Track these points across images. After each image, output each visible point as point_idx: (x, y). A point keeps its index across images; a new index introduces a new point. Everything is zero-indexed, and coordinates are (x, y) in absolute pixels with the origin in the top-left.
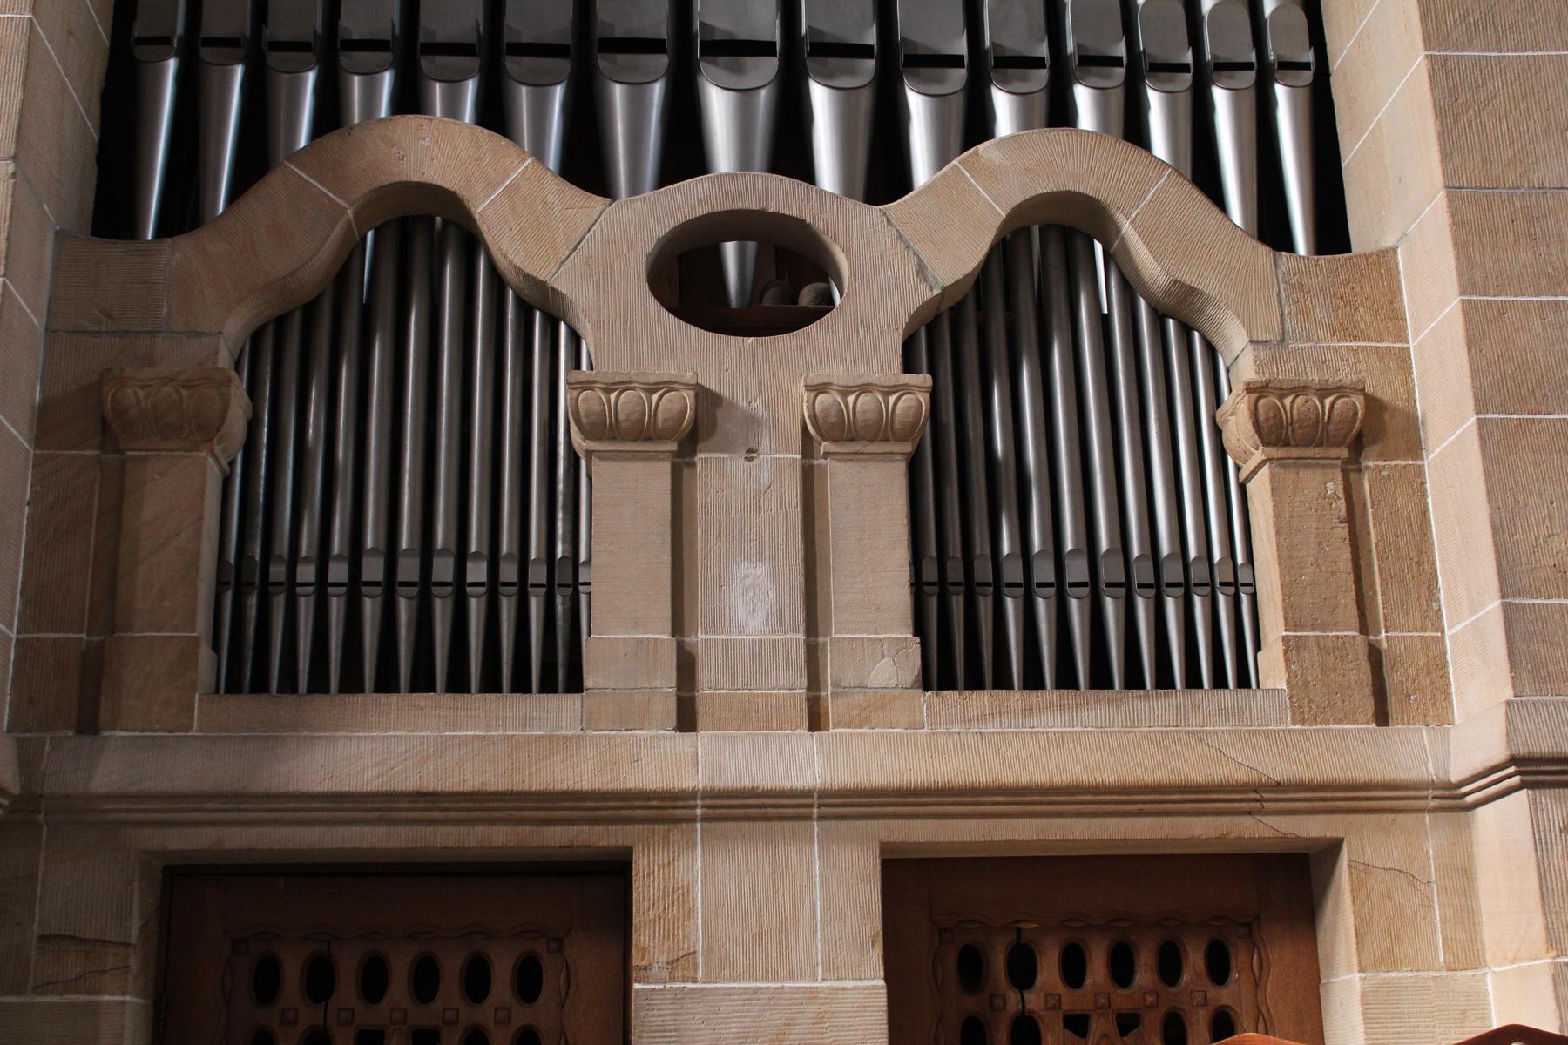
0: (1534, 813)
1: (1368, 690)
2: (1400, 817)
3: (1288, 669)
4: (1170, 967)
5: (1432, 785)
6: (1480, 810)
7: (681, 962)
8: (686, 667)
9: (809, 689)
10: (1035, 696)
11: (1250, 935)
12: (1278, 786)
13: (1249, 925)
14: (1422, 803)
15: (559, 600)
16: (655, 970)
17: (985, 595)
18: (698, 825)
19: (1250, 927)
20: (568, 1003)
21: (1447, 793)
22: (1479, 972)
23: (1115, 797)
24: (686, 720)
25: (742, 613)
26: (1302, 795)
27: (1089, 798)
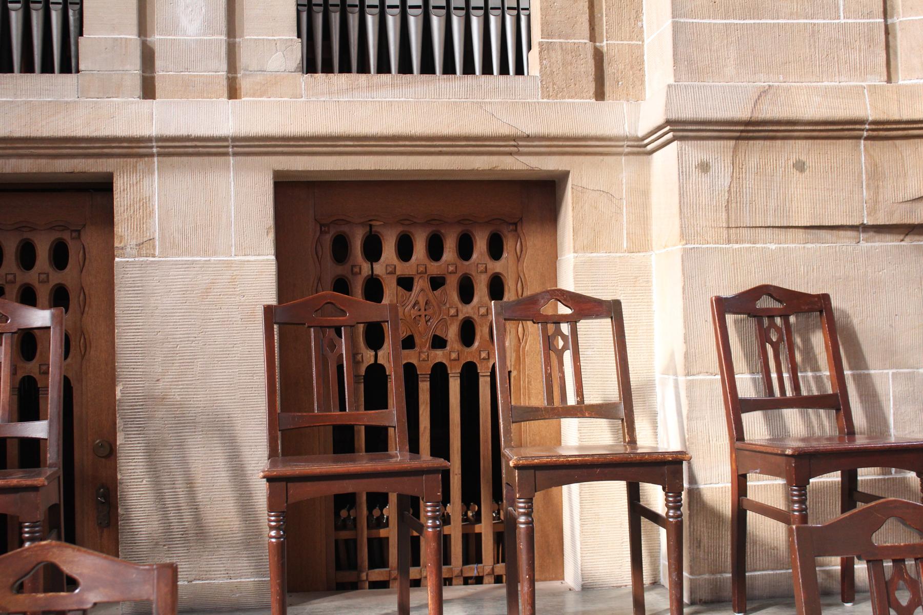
0: (680, 156)
1: (591, 78)
2: (606, 158)
3: (541, 63)
4: (465, 249)
5: (626, 138)
6: (655, 154)
7: (145, 245)
8: (148, 57)
10: (384, 77)
11: (516, 230)
12: (528, 138)
13: (516, 224)
14: (620, 150)
15: (71, 13)
16: (128, 250)
17: (353, 13)
19: (515, 224)
20: (84, 271)
21: (636, 143)
22: (648, 254)
24: (148, 90)
25: (184, 22)
26: (543, 143)
27: (407, 143)
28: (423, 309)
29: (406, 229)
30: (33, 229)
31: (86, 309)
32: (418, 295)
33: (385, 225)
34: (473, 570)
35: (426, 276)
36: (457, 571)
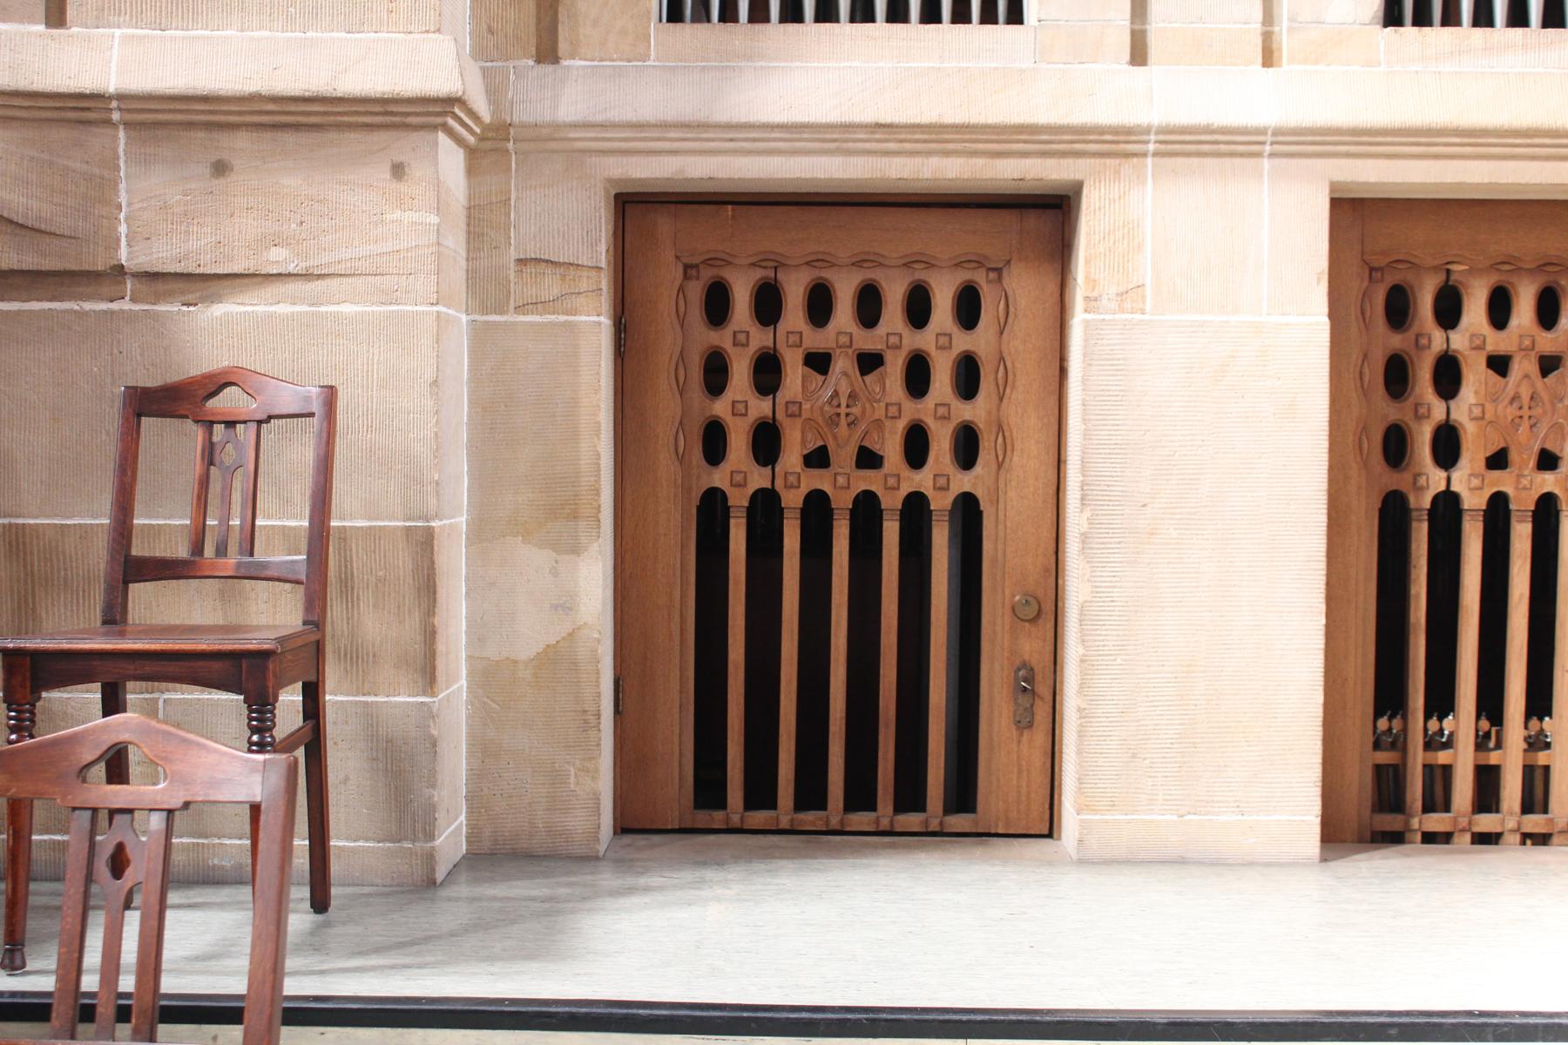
9: (1264, 24)
16: (1105, 301)
18: (122, 134)
23: (1389, 139)
28: (1526, 407)
29: (1504, 278)
30: (930, 266)
31: (1008, 390)
32: (1518, 386)
33: (1472, 271)
34: (1486, 822)
35: (850, 351)
36: (1511, 824)
